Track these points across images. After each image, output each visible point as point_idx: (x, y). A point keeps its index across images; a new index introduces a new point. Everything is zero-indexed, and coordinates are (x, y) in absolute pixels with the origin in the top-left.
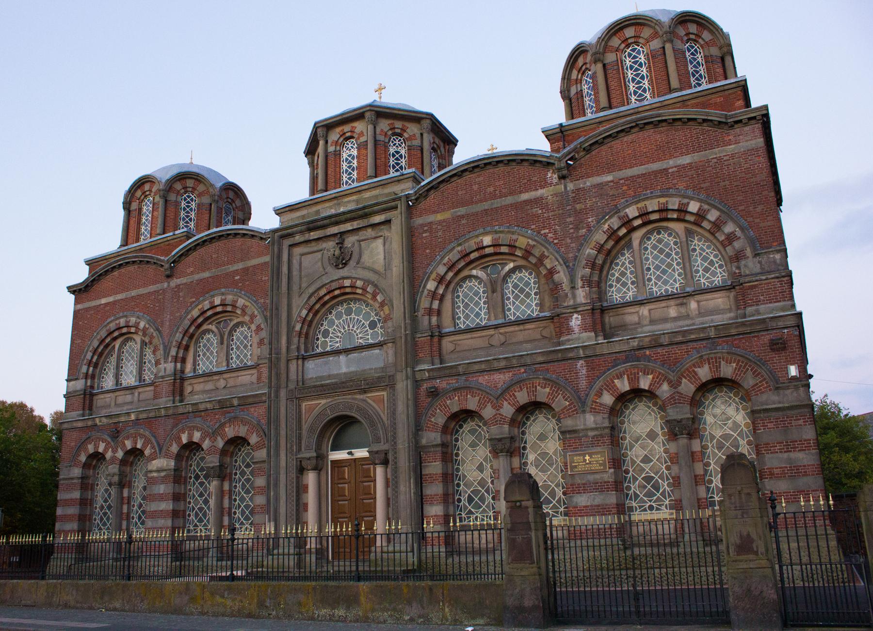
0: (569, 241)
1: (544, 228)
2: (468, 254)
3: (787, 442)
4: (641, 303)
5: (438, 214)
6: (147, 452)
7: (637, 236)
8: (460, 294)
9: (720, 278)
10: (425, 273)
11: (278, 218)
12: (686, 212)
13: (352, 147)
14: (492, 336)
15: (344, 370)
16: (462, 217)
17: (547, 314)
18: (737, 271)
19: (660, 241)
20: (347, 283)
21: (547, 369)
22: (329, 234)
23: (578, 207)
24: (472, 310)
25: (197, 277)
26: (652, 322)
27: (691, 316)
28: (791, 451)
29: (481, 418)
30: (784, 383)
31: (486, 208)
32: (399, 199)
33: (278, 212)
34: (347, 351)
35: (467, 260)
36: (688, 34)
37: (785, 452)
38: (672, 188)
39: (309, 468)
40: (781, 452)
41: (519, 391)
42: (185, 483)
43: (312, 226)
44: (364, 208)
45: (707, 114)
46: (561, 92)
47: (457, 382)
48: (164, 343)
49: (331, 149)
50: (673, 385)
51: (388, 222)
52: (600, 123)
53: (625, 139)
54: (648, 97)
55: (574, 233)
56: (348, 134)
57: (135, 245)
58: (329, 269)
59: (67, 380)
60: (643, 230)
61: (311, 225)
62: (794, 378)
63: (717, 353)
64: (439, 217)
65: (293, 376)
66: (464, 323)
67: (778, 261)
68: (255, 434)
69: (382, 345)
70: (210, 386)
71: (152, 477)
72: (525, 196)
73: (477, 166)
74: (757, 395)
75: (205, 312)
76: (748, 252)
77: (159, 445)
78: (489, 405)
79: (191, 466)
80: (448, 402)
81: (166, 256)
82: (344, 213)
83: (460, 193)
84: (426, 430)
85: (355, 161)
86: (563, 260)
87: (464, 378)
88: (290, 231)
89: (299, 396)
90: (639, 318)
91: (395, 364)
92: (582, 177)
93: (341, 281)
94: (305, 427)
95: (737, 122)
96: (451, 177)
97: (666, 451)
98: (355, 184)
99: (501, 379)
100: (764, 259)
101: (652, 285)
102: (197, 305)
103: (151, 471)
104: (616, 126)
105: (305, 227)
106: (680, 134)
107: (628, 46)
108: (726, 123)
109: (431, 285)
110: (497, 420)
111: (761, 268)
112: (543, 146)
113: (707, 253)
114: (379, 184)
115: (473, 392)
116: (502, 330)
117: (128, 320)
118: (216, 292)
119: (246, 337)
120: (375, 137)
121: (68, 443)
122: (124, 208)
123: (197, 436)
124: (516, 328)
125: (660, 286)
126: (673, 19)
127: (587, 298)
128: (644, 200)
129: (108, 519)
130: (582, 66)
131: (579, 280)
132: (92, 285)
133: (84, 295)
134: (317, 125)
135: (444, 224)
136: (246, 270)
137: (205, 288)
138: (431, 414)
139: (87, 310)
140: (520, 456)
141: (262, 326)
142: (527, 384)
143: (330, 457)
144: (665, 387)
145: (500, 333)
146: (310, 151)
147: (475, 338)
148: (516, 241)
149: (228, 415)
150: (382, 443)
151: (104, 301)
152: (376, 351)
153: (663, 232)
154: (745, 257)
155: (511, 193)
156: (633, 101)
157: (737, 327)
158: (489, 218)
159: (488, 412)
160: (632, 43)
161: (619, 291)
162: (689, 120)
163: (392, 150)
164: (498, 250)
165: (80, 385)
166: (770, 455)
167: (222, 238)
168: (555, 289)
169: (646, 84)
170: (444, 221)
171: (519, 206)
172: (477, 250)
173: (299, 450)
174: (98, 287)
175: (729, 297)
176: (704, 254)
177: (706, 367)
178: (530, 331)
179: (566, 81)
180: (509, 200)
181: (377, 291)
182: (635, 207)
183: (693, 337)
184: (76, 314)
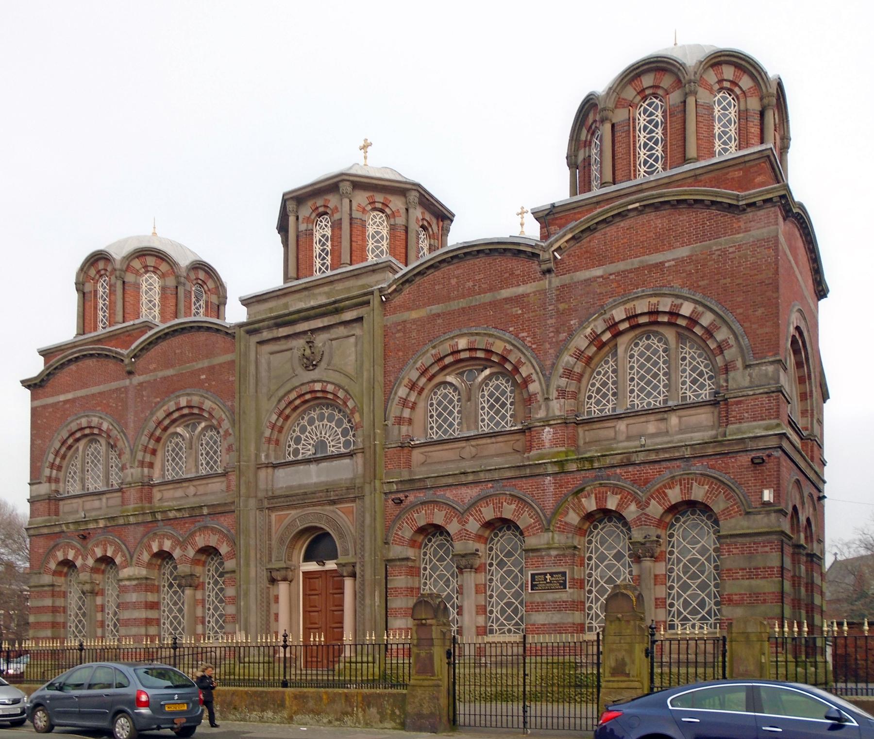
0: (547, 346)
1: (523, 330)
2: (441, 359)
3: (750, 569)
4: (619, 417)
5: (413, 312)
6: (118, 560)
7: (623, 341)
8: (434, 402)
9: (707, 392)
10: (396, 379)
11: (245, 309)
12: (678, 315)
13: (326, 226)
14: (463, 448)
15: (314, 480)
16: (438, 315)
17: (519, 427)
18: (725, 384)
19: (648, 348)
20: (318, 387)
21: (515, 485)
22: (298, 331)
23: (562, 306)
24: (445, 420)
25: (161, 374)
26: (629, 438)
27: (670, 432)
28: (753, 578)
29: (517, 527)
30: (756, 508)
31: (464, 305)
32: (372, 293)
33: (245, 302)
34: (317, 460)
35: (441, 364)
36: (720, 81)
37: (747, 579)
38: (666, 286)
39: (345, 574)
40: (743, 579)
41: (485, 507)
42: (158, 591)
43: (281, 322)
44: (335, 302)
45: (717, 194)
46: (567, 158)
47: (425, 496)
48: (130, 447)
49: (303, 227)
50: (641, 506)
51: (360, 319)
52: (598, 203)
53: (622, 224)
54: (660, 169)
55: (553, 337)
56: (321, 210)
57: (92, 334)
58: (300, 370)
59: (29, 484)
60: (631, 335)
61: (279, 320)
62: (768, 504)
63: (691, 474)
64: (414, 315)
65: (262, 485)
66: (437, 433)
67: (770, 374)
68: (225, 544)
69: (352, 455)
70: (179, 493)
71: (124, 586)
72: (506, 293)
73: (456, 256)
74: (726, 519)
75: (658, 313)
76: (739, 364)
77: (130, 553)
78: (455, 520)
79: (164, 574)
80: (415, 515)
81: (127, 349)
82: (313, 308)
83: (437, 287)
84: (393, 543)
85: (329, 244)
86: (540, 368)
87: (431, 492)
88: (256, 326)
89: (268, 506)
90: (616, 434)
91: (364, 476)
92: (569, 271)
93: (311, 384)
94: (274, 537)
95: (749, 205)
96: (428, 268)
97: (630, 573)
98: (329, 273)
99: (470, 494)
100: (755, 371)
101: (634, 398)
102: (163, 406)
103: (121, 580)
104: (612, 209)
105: (273, 321)
106: (684, 219)
107: (644, 99)
108: (738, 206)
109: (402, 392)
110: (643, 520)
111: (751, 381)
112: (532, 230)
113: (698, 363)
114: (353, 273)
115: (417, 510)
116: (473, 443)
117: (90, 420)
118: (181, 392)
119: (215, 442)
120: (351, 215)
121: (36, 550)
122: (77, 290)
123: (167, 545)
124: (489, 441)
125: (643, 399)
126: (701, 62)
127: (560, 411)
128: (633, 299)
129: (83, 627)
130: (592, 124)
131: (555, 391)
132: (48, 380)
133: (40, 391)
134: (286, 197)
135: (419, 323)
136: (211, 369)
137: (169, 388)
138: (398, 528)
139: (45, 407)
140: (486, 573)
141: (230, 431)
142: (493, 500)
143: (301, 568)
144: (633, 507)
145: (472, 446)
146: (283, 228)
147: (447, 450)
148: (492, 345)
149: (197, 524)
150: (350, 556)
151: (62, 398)
152: (347, 461)
153: (652, 337)
154: (735, 368)
155: (491, 290)
156: (642, 173)
157: (714, 447)
158: (466, 318)
159: (453, 528)
160: (650, 95)
161: (598, 403)
162: (696, 201)
163: (371, 230)
164: (474, 355)
165: (44, 489)
166: (731, 582)
167: (185, 331)
168: (529, 400)
169: (659, 151)
170: (419, 319)
171: (494, 304)
172: (470, 350)
173: (270, 560)
174: (53, 381)
175: (713, 413)
176: (695, 363)
177: (677, 489)
178: (502, 444)
179: (574, 142)
180: (487, 297)
181: (348, 397)
182: (622, 308)
183: (667, 455)
184: (34, 412)
